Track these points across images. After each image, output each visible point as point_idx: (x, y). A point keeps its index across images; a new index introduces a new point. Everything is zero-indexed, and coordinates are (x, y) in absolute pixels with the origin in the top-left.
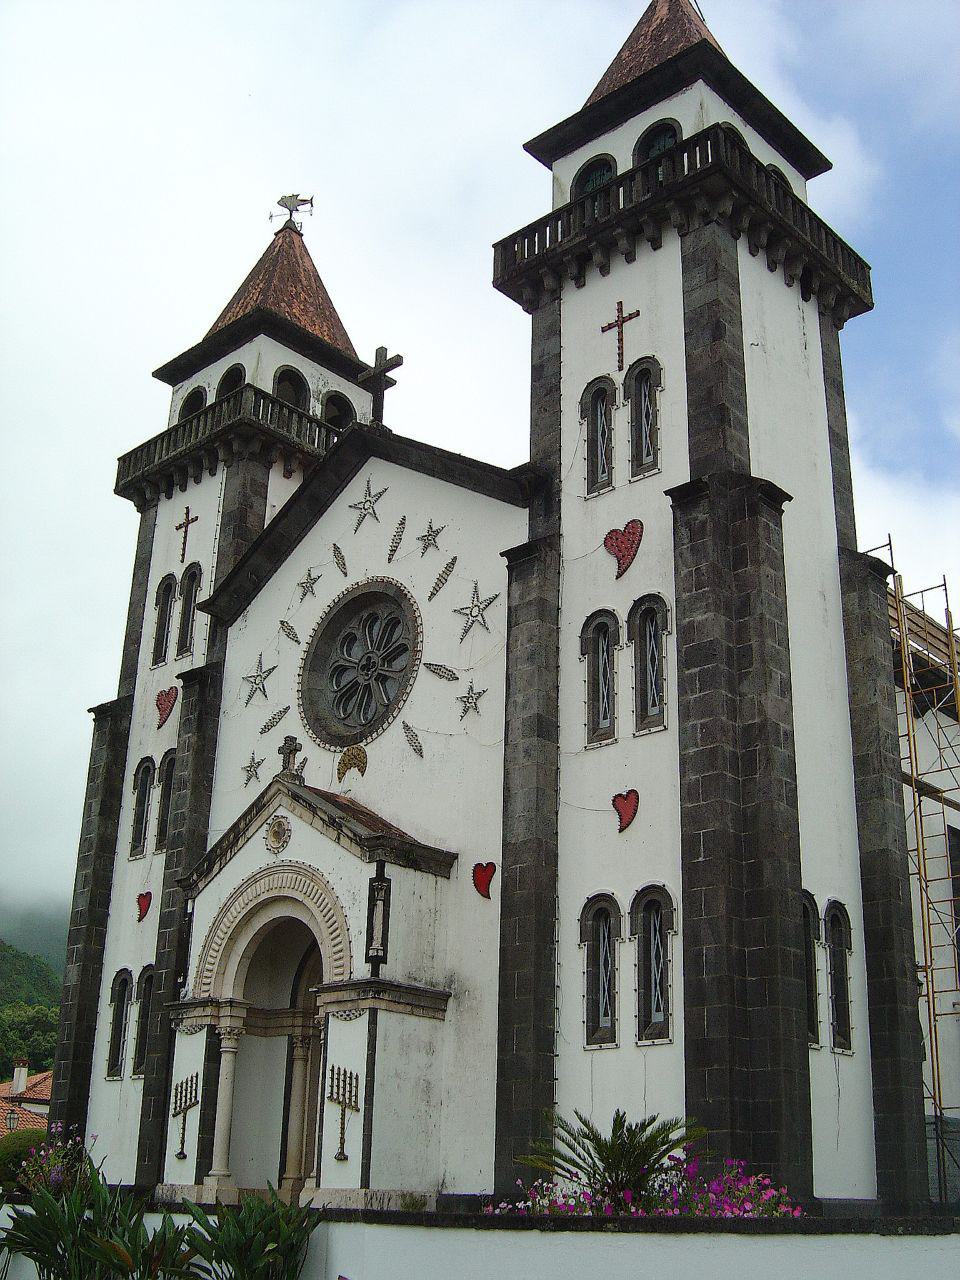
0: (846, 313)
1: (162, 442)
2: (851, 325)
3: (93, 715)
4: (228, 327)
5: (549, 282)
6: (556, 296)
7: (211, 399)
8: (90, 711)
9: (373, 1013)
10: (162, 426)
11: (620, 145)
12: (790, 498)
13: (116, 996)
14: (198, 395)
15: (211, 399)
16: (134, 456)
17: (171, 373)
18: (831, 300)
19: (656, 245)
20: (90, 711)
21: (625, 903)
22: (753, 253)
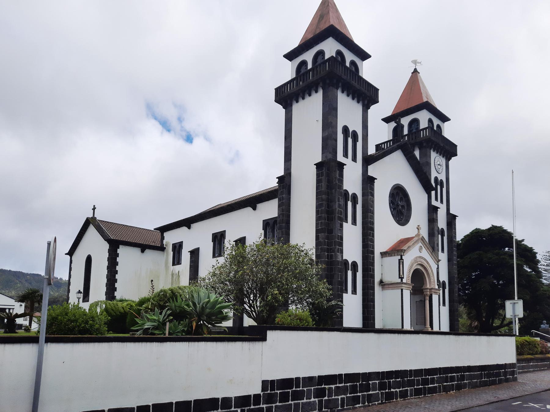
0: (370, 104)
1: (320, 67)
2: (373, 107)
3: (190, 253)
4: (301, 44)
5: (289, 102)
6: (291, 105)
7: (310, 66)
8: (189, 252)
9: (402, 290)
10: (289, 79)
11: (308, 56)
12: (346, 165)
13: (347, 268)
14: (304, 63)
15: (310, 66)
16: (279, 90)
17: (290, 56)
18: (366, 102)
19: (316, 92)
20: (189, 252)
21: (174, 403)
22: (343, 92)
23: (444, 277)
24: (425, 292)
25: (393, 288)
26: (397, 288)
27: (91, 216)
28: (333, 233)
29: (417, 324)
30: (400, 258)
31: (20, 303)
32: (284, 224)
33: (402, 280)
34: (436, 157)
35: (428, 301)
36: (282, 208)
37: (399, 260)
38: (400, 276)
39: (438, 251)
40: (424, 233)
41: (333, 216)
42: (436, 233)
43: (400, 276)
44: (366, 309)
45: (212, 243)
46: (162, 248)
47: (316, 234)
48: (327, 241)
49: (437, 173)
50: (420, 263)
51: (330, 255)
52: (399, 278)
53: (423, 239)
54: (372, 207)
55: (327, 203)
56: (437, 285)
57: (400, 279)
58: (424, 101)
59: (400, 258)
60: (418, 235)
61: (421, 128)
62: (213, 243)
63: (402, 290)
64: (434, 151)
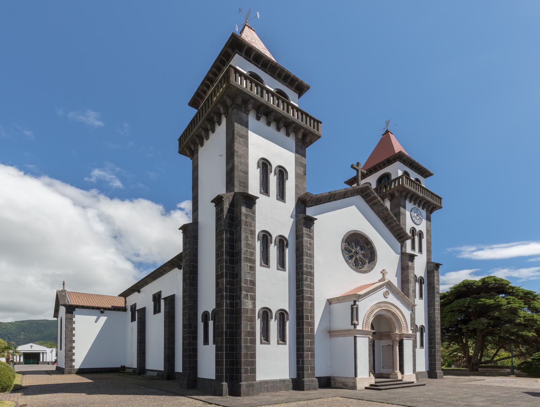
23: (421, 320)
24: (393, 337)
25: (344, 335)
26: (350, 335)
27: (61, 289)
28: (238, 278)
29: (384, 367)
30: (353, 304)
31: (51, 349)
32: (188, 275)
33: (355, 327)
34: (413, 208)
35: (398, 347)
36: (186, 259)
37: (352, 305)
38: (353, 323)
39: (415, 296)
40: (394, 279)
41: (238, 258)
42: (412, 279)
43: (353, 323)
44: (301, 359)
45: (153, 303)
46: (124, 309)
47: (216, 280)
48: (229, 287)
49: (411, 210)
50: (386, 308)
51: (235, 302)
52: (352, 324)
53: (389, 285)
54: (310, 250)
55: (229, 244)
56: (411, 329)
57: (353, 326)
58: (396, 152)
59: (353, 304)
60: (383, 279)
61: (392, 179)
62: (153, 302)
63: (355, 338)
64: (410, 202)
